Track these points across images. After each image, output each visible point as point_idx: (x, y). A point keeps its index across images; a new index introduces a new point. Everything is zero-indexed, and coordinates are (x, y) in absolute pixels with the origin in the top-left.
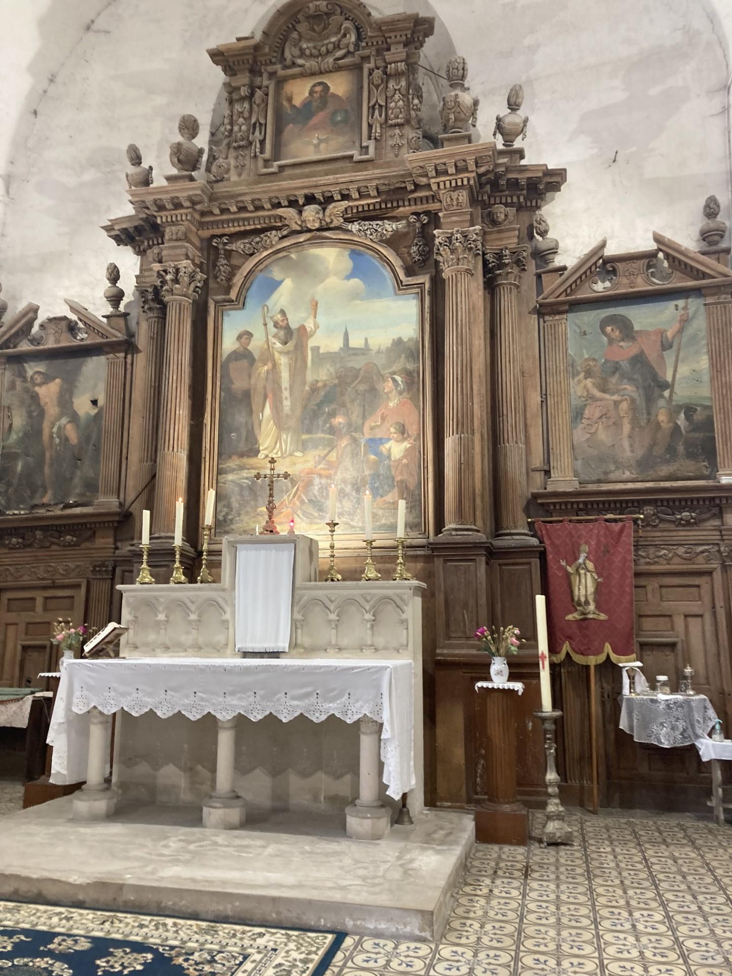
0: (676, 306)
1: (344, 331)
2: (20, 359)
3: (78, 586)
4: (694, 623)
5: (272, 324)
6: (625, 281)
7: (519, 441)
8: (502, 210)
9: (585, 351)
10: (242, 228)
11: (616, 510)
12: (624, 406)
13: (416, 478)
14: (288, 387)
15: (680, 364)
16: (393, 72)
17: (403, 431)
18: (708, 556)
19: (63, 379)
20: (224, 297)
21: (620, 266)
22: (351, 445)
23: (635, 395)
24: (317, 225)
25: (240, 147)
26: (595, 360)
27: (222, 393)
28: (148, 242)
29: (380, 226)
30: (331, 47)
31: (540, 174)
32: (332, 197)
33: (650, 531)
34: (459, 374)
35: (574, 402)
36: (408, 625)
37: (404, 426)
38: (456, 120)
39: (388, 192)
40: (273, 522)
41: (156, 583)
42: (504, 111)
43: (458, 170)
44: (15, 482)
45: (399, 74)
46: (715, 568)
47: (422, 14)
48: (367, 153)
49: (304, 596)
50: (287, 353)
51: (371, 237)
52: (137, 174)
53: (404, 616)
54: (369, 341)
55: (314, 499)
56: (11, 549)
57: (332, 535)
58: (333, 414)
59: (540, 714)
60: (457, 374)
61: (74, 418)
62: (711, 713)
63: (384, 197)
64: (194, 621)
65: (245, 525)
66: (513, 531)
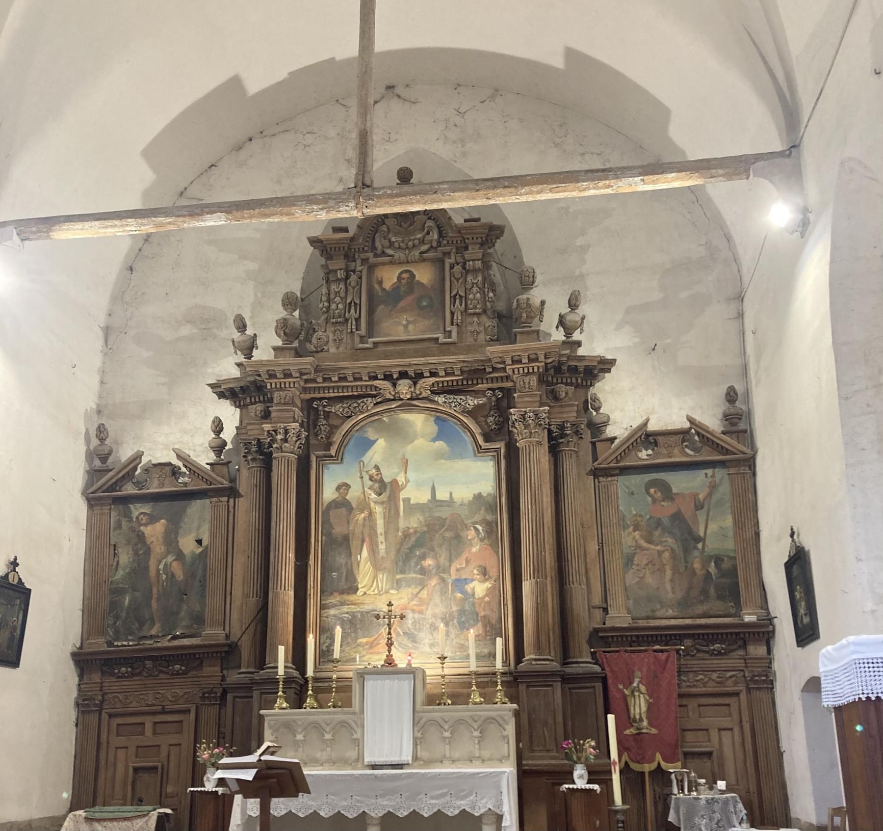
0: (706, 474)
2: (126, 500)
3: (188, 711)
4: (726, 737)
5: (368, 477)
6: (664, 451)
8: (564, 389)
9: (633, 509)
10: (341, 394)
11: (662, 642)
12: (666, 555)
13: (497, 614)
14: (383, 532)
15: (709, 523)
16: (471, 268)
18: (735, 680)
19: (168, 520)
21: (660, 439)
22: (439, 584)
23: (675, 547)
24: (409, 396)
25: (337, 323)
26: (641, 516)
28: (251, 400)
29: (464, 401)
30: (416, 242)
31: (596, 364)
33: (689, 660)
35: (626, 551)
36: (508, 740)
37: (485, 569)
38: (527, 317)
40: (392, 656)
41: (291, 708)
42: (565, 309)
43: (530, 360)
44: (124, 615)
46: (742, 690)
47: (495, 222)
48: (450, 337)
49: (422, 718)
52: (244, 342)
53: (505, 733)
54: (453, 495)
56: (119, 677)
57: (443, 667)
58: (423, 557)
59: (614, 808)
60: (532, 529)
61: (180, 556)
62: (740, 806)
64: (328, 740)
66: (579, 660)
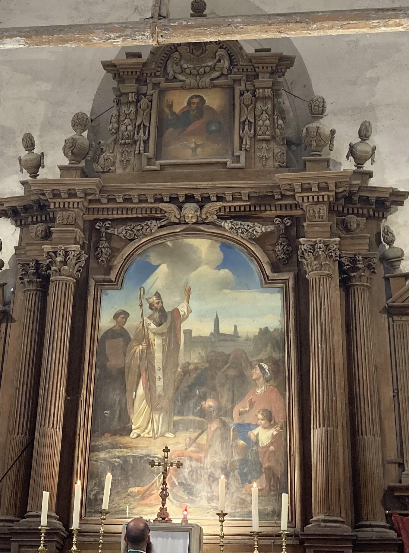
1: (215, 317)
5: (148, 305)
7: (375, 434)
14: (161, 368)
16: (261, 96)
17: (270, 418)
20: (103, 277)
25: (125, 144)
27: (98, 371)
28: (32, 219)
30: (208, 69)
31: (388, 196)
32: (209, 197)
34: (324, 369)
37: (270, 413)
39: (257, 197)
43: (320, 189)
45: (266, 98)
48: (238, 162)
50: (161, 335)
51: (242, 235)
55: (184, 481)
57: (222, 526)
58: (204, 398)
63: (253, 202)
65: (116, 505)
66: (373, 523)
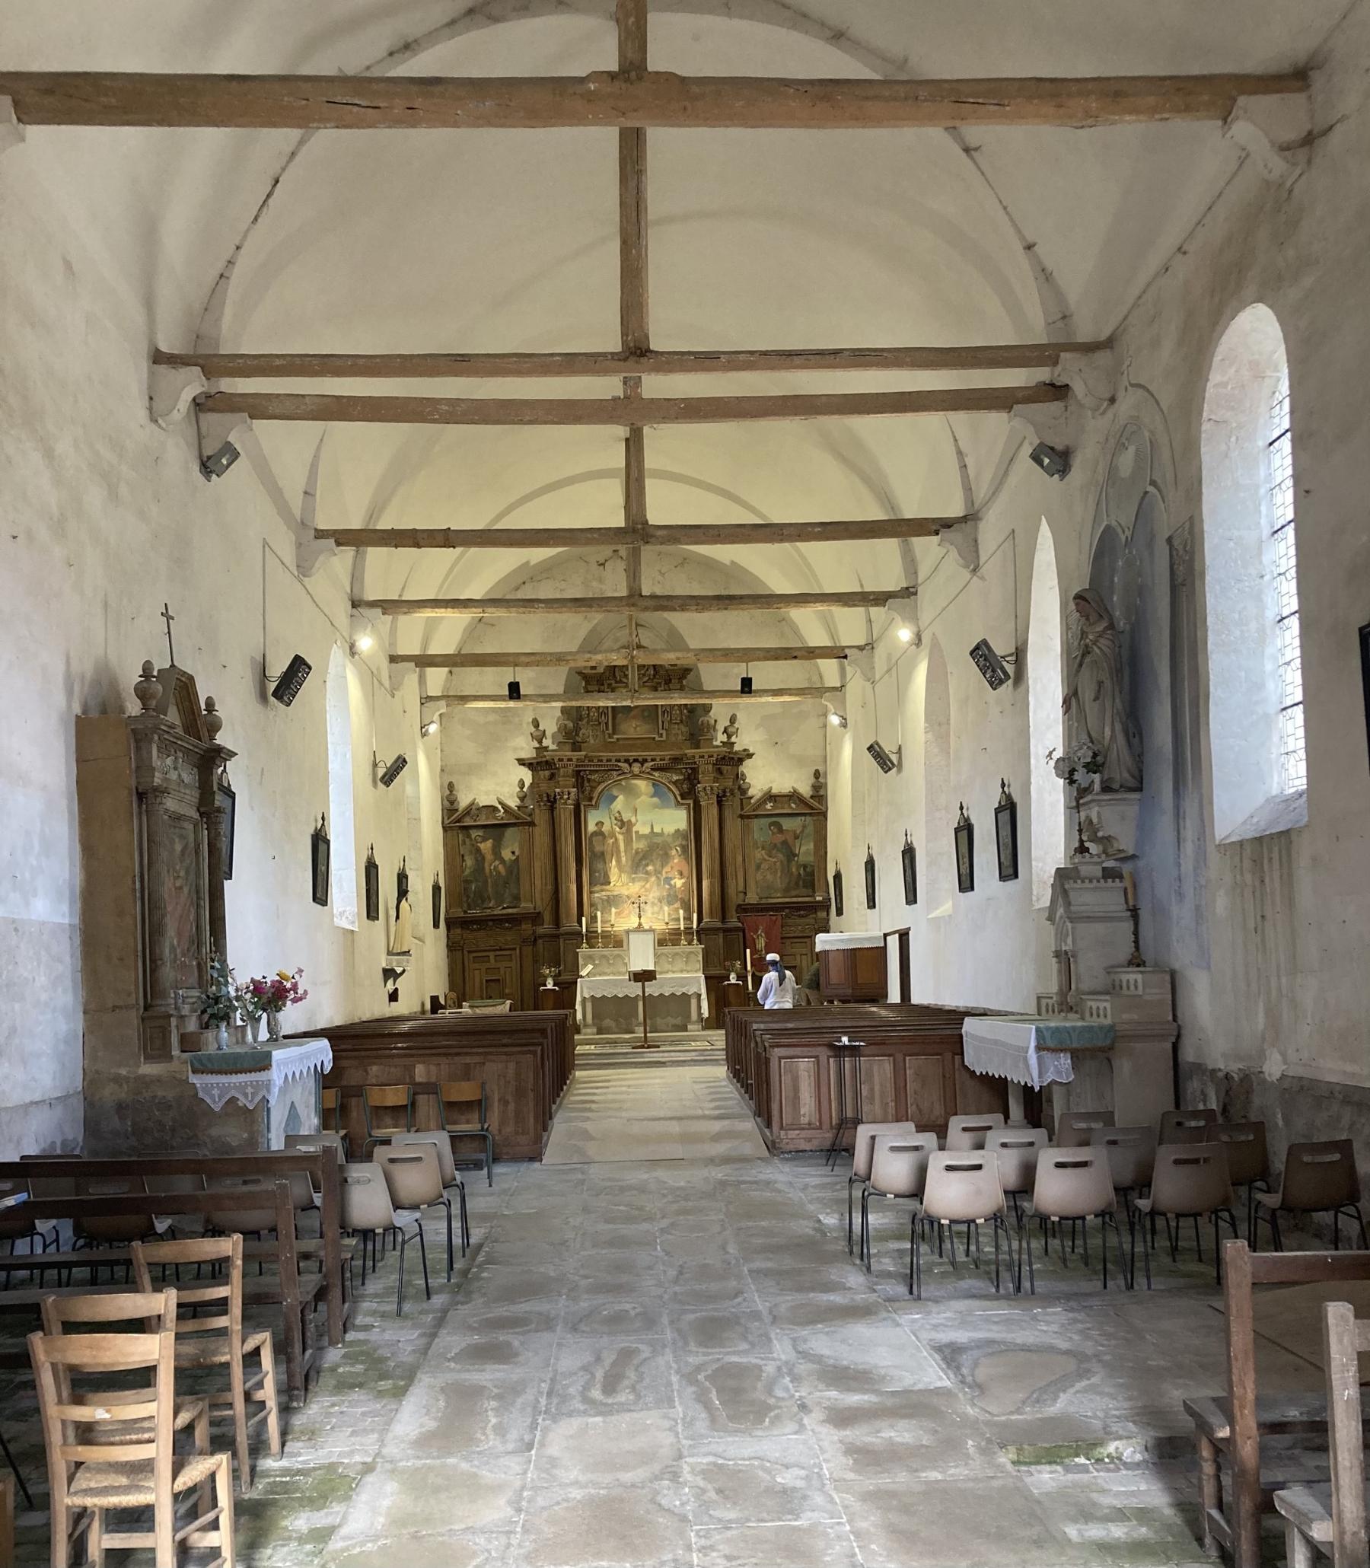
17: (681, 874)
58: (647, 865)
61: (502, 861)
